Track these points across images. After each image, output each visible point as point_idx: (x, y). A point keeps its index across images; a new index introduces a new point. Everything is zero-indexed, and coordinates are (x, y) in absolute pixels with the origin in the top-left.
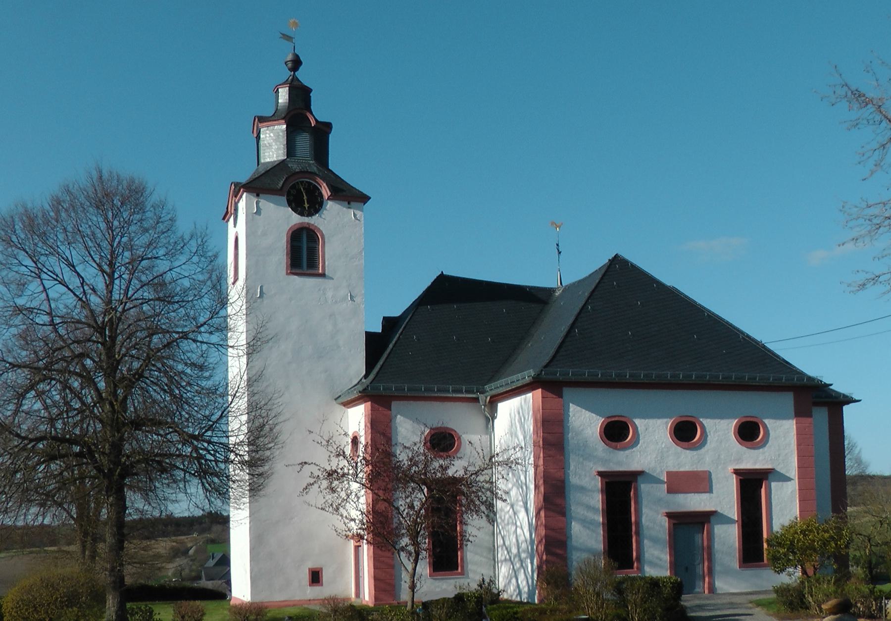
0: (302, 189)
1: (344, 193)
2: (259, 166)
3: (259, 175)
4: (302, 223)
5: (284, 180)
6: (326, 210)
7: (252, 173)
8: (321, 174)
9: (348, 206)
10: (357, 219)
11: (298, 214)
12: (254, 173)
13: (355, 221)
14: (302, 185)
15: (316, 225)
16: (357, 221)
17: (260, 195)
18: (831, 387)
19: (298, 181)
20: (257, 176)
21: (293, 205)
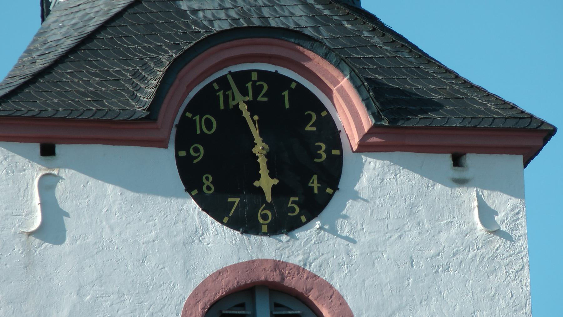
0: (243, 107)
1: (436, 117)
2: (50, 19)
3: (52, 57)
4: (251, 264)
5: (160, 72)
6: (356, 196)
7: (20, 51)
8: (324, 34)
9: (458, 173)
10: (497, 232)
11: (234, 224)
12: (29, 52)
13: (486, 243)
14: (244, 92)
15: (313, 268)
16: (499, 242)
17: (59, 149)
18: (65, 218)
19: (224, 72)
20: (40, 65)
21: (207, 181)
